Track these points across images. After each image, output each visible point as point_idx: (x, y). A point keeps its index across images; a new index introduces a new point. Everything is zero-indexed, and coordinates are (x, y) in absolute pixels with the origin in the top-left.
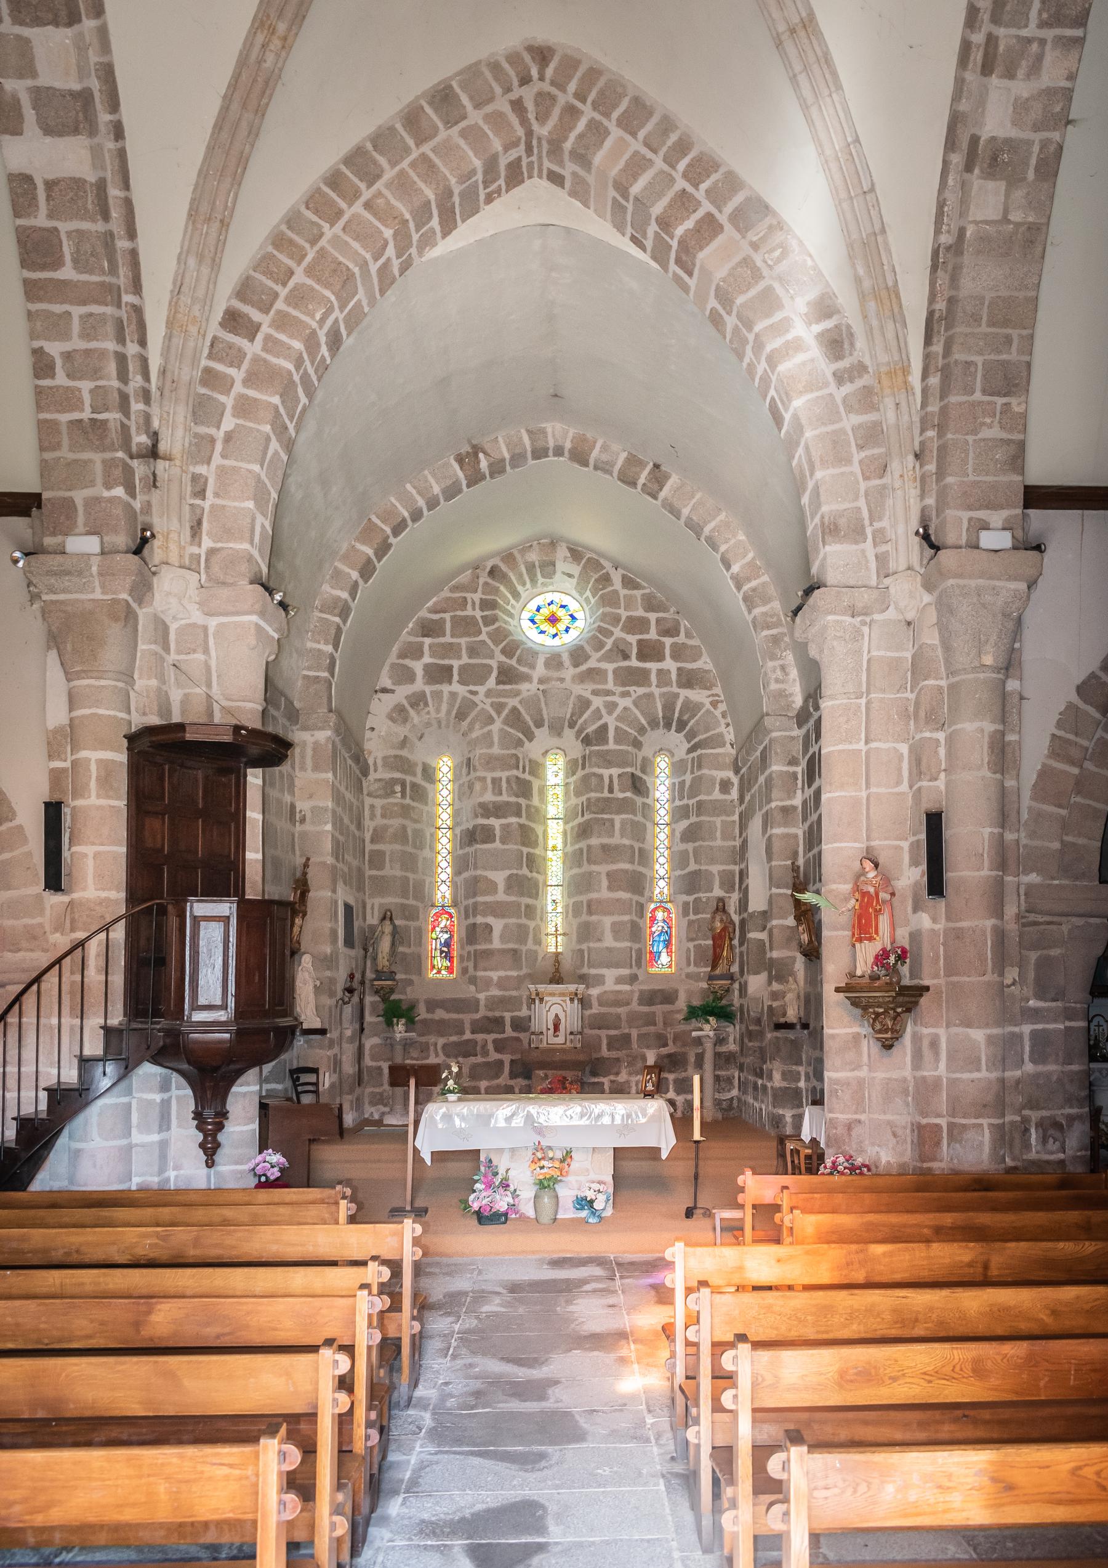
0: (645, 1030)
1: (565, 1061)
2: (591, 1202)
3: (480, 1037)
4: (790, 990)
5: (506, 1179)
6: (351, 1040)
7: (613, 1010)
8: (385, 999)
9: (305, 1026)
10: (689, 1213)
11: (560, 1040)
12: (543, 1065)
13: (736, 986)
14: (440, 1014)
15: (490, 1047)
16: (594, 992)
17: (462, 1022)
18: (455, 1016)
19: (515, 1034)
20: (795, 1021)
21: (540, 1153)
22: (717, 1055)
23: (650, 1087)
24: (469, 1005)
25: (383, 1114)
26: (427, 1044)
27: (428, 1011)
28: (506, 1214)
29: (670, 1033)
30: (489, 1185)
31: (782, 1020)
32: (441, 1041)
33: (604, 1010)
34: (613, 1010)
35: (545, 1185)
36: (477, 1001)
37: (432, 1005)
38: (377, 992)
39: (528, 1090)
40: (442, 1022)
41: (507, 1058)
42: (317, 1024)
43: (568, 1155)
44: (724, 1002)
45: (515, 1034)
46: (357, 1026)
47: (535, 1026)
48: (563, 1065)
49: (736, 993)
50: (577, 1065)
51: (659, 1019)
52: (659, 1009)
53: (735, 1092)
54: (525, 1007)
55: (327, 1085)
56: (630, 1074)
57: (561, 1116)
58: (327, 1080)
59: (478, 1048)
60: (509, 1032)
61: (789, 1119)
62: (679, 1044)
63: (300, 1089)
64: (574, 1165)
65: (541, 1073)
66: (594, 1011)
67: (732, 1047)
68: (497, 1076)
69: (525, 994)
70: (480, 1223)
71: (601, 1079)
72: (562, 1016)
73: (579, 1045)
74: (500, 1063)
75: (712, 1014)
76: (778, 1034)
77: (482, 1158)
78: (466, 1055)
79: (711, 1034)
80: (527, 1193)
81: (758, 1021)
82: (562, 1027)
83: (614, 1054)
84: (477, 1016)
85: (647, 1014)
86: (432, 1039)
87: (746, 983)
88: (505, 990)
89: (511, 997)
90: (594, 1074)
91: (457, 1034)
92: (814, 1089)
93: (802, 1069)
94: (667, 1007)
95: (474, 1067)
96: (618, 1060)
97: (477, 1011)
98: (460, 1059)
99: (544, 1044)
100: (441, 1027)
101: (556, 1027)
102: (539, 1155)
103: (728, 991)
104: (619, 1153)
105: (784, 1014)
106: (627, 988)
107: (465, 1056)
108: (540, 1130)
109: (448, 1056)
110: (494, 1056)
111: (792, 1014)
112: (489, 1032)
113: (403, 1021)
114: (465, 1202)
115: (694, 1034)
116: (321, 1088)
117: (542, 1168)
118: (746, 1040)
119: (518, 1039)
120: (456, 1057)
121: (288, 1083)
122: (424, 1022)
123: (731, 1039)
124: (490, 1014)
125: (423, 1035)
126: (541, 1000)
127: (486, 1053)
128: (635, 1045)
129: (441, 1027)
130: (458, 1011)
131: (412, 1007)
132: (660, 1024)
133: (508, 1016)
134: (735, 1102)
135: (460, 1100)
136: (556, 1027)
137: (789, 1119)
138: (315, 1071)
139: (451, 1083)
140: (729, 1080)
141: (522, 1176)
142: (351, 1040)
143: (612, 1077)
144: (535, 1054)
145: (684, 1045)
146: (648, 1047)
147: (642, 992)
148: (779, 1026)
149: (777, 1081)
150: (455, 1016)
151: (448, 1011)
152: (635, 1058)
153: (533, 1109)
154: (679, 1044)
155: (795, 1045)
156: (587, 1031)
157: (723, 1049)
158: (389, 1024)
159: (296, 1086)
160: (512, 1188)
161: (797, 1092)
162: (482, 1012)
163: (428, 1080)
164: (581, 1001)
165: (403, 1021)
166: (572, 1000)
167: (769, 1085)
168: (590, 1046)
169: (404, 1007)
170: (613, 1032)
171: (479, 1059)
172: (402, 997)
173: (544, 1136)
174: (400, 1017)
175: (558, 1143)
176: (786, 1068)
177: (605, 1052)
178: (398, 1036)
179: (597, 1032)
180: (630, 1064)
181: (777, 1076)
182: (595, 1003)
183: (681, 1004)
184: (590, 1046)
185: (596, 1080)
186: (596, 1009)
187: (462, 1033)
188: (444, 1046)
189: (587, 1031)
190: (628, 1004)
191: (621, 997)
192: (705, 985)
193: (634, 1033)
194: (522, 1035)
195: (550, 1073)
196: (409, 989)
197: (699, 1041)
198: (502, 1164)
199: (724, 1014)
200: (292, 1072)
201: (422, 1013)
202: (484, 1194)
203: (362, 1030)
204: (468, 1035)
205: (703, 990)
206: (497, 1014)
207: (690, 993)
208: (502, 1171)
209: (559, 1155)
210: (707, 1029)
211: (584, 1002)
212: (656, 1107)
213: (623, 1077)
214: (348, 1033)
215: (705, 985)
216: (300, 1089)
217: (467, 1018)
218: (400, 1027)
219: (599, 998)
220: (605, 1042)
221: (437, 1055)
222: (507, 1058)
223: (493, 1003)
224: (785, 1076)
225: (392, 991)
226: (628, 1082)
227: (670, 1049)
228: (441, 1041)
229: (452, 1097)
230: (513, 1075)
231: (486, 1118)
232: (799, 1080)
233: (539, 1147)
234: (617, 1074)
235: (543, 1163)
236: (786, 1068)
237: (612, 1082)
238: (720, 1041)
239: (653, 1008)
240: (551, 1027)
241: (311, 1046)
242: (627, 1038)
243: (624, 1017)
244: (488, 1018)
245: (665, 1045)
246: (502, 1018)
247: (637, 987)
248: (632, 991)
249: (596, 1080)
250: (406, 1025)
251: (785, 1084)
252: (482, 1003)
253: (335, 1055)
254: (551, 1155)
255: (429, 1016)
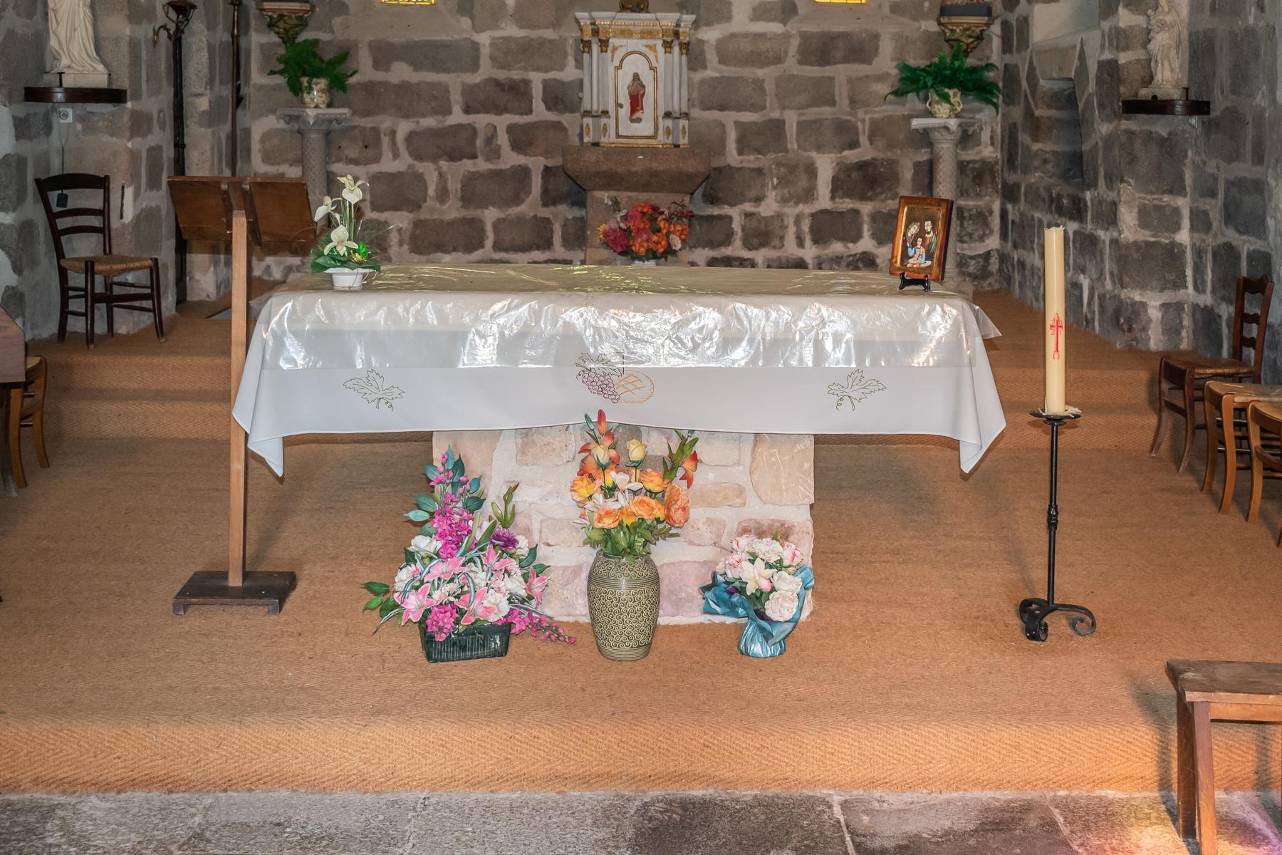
0: (813, 113)
1: (654, 174)
2: (760, 597)
3: (481, 120)
4: (1163, 26)
5: (506, 520)
6: (211, 119)
7: (748, 72)
8: (288, 38)
9: (68, 82)
10: (1034, 617)
11: (645, 128)
12: (613, 181)
13: (996, 29)
14: (400, 72)
15: (503, 140)
16: (711, 35)
17: (445, 89)
18: (431, 77)
19: (552, 116)
20: (1176, 94)
21: (604, 446)
22: (962, 167)
23: (918, 259)
24: (467, 57)
25: (289, 269)
26: (376, 131)
27: (377, 65)
28: (505, 629)
29: (863, 120)
30: (454, 539)
31: (1145, 93)
32: (404, 127)
33: (729, 71)
34: (748, 72)
35: (622, 546)
36: (476, 47)
37: (384, 55)
38: (271, 25)
39: (577, 237)
40: (403, 88)
41: (536, 163)
42: (97, 77)
43: (682, 456)
44: (970, 61)
45: (552, 116)
46: (227, 92)
47: (591, 100)
48: (651, 181)
49: (996, 43)
50: (679, 182)
51: (841, 92)
52: (841, 72)
53: (993, 242)
54: (571, 61)
55: (129, 215)
56: (783, 201)
57: (666, 337)
58: (128, 206)
59: (479, 143)
60: (540, 111)
61: (1154, 313)
62: (881, 143)
63: (63, 223)
64: (704, 477)
65: (605, 197)
66: (710, 73)
67: (988, 151)
68: (517, 199)
69: (571, 35)
70: (429, 657)
71: (726, 210)
72: (647, 78)
73: (684, 141)
74: (524, 172)
75: (952, 82)
76: (1126, 124)
77: (437, 454)
78: (454, 156)
79: (953, 123)
80: (569, 556)
81: (1067, 99)
82: (648, 102)
83: (751, 161)
84: (476, 78)
85: (818, 82)
86: (385, 122)
87: (1025, 22)
88: (532, 26)
89: (542, 43)
90: (712, 199)
91: (435, 112)
92: (1227, 254)
93: (1183, 203)
94: (859, 69)
95: (470, 180)
96: (759, 171)
97: (475, 67)
98: (443, 164)
99: (610, 139)
100: (405, 99)
101: (636, 102)
102: (602, 453)
103: (980, 38)
104: (820, 440)
105: (1149, 79)
106: (776, 28)
107: (452, 158)
108: (602, 382)
109: (419, 157)
110: (510, 159)
111: (1169, 77)
112: (500, 110)
113: (322, 83)
114: (382, 589)
115: (917, 123)
116: (115, 223)
117: (610, 491)
118: (1024, 138)
119: (558, 126)
120: (434, 159)
121: (33, 210)
122: (370, 88)
123: (985, 136)
124: (502, 75)
125: (367, 113)
126: (604, 44)
127: (494, 154)
128: (792, 144)
129: (405, 99)
130: (436, 67)
131: (344, 55)
132: (844, 102)
133: (537, 80)
134: (994, 265)
135: (368, 287)
136: (636, 102)
137: (1154, 313)
138: (101, 183)
139: (340, 234)
140: (982, 217)
141: (553, 509)
142: (211, 119)
143: (748, 207)
144: (591, 157)
145: (890, 146)
146: (820, 148)
147: (805, 38)
148: (1134, 107)
149: (1130, 227)
150: (431, 77)
151: (417, 67)
152: (792, 169)
153: (579, 316)
154: (881, 143)
155: (1169, 148)
156: (696, 113)
157: (969, 155)
158: (296, 89)
159: (52, 217)
160: (523, 545)
161: (1173, 254)
162: (487, 70)
163: (288, 232)
164: (685, 47)
165: (322, 83)
166: (668, 46)
167: (1104, 235)
168: (707, 143)
169: (328, 56)
170: (749, 117)
171: (482, 165)
172: (324, 36)
173: (615, 398)
174: (315, 74)
175: (661, 414)
176: (1149, 199)
177: (732, 157)
178: (311, 113)
179: (715, 114)
180: (784, 182)
181: (1128, 218)
182: (711, 57)
183: (886, 62)
184: (707, 143)
185: (716, 211)
186: (713, 71)
187: (446, 110)
188: (410, 138)
189: (696, 113)
190: (778, 60)
191: (763, 46)
192: (932, 26)
193: (792, 119)
194: (565, 119)
195: (624, 196)
196: (337, 21)
197: (925, 138)
198: (496, 471)
199: (976, 86)
200: (44, 186)
201: (364, 71)
202: (439, 568)
203: (239, 100)
204: (457, 117)
205: (928, 36)
206: (516, 75)
207: (902, 43)
208: (494, 492)
209: (659, 447)
210: (944, 115)
211: (693, 54)
212: (942, 321)
213: (769, 207)
214: (203, 104)
215: (932, 26)
216: (63, 223)
217: (455, 82)
218: (317, 95)
219: (721, 45)
220: (732, 136)
221: (396, 155)
222: (536, 163)
223: (508, 53)
224: (1145, 217)
225: (303, 23)
226: (779, 216)
227: (865, 152)
228: (404, 127)
229: (346, 278)
230: (549, 199)
231: (450, 343)
232: (1177, 227)
233: (600, 430)
234: (758, 200)
235: (613, 477)
236: (1149, 199)
237: (748, 215)
238: (966, 138)
239: (828, 71)
240: (625, 100)
241: (90, 128)
242: (777, 127)
243: (770, 87)
244: (497, 83)
245: (854, 144)
246: (527, 83)
247: (794, 27)
248: (787, 36)
249: (716, 211)
250: (329, 90)
251: (1146, 236)
252: (485, 52)
253: (154, 152)
254: (636, 453)
255: (380, 76)
